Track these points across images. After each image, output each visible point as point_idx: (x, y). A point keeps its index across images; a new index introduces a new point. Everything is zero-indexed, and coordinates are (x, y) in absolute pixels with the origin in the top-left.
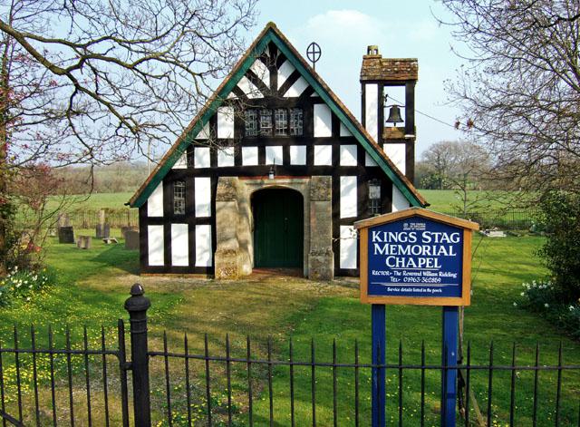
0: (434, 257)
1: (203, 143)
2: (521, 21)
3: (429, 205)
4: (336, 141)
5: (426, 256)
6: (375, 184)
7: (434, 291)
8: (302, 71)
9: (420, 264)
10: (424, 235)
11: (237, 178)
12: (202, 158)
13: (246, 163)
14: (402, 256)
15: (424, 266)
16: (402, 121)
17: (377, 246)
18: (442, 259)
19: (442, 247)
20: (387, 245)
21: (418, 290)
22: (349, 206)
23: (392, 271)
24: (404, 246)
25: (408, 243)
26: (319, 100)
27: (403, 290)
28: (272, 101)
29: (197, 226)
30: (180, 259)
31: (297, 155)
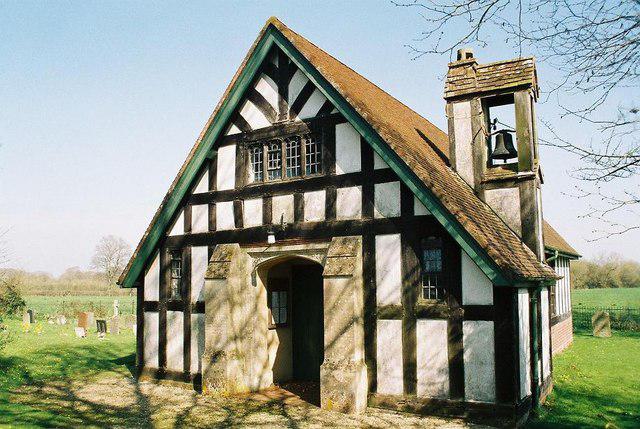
11: (237, 245)
26: (341, 119)
29: (376, 237)
31: (315, 205)
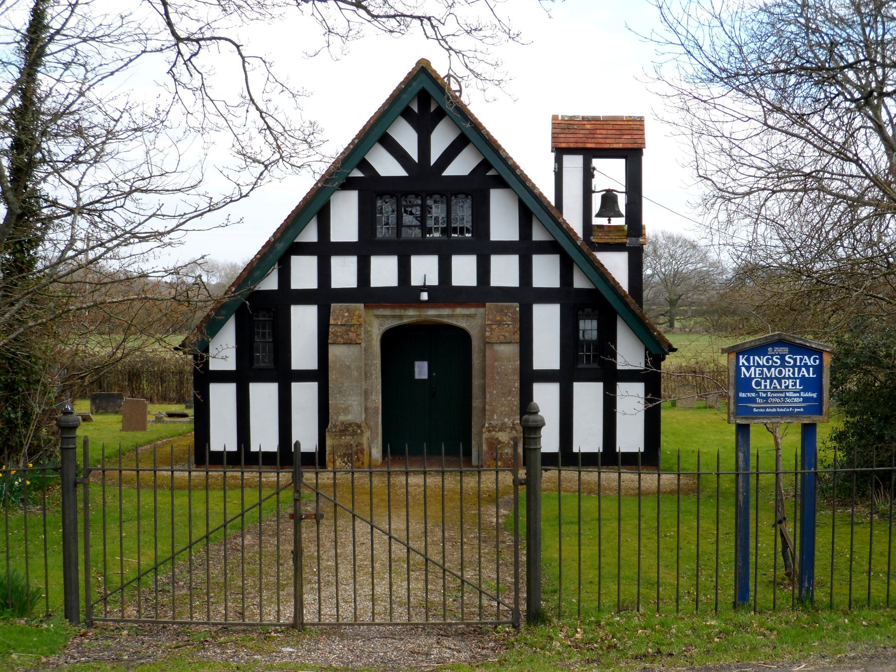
0: (796, 378)
1: (304, 249)
2: (803, 67)
3: (675, 350)
4: (525, 249)
5: (789, 378)
6: (588, 317)
7: (796, 410)
8: (471, 134)
9: (783, 385)
10: (787, 358)
12: (304, 273)
13: (496, 280)
14: (767, 378)
15: (787, 387)
16: (620, 215)
17: (743, 369)
18: (803, 380)
19: (803, 369)
20: (753, 368)
21: (782, 410)
22: (547, 353)
23: (757, 392)
24: (769, 368)
25: (772, 366)
27: (767, 410)
28: (424, 179)
30: (265, 438)
